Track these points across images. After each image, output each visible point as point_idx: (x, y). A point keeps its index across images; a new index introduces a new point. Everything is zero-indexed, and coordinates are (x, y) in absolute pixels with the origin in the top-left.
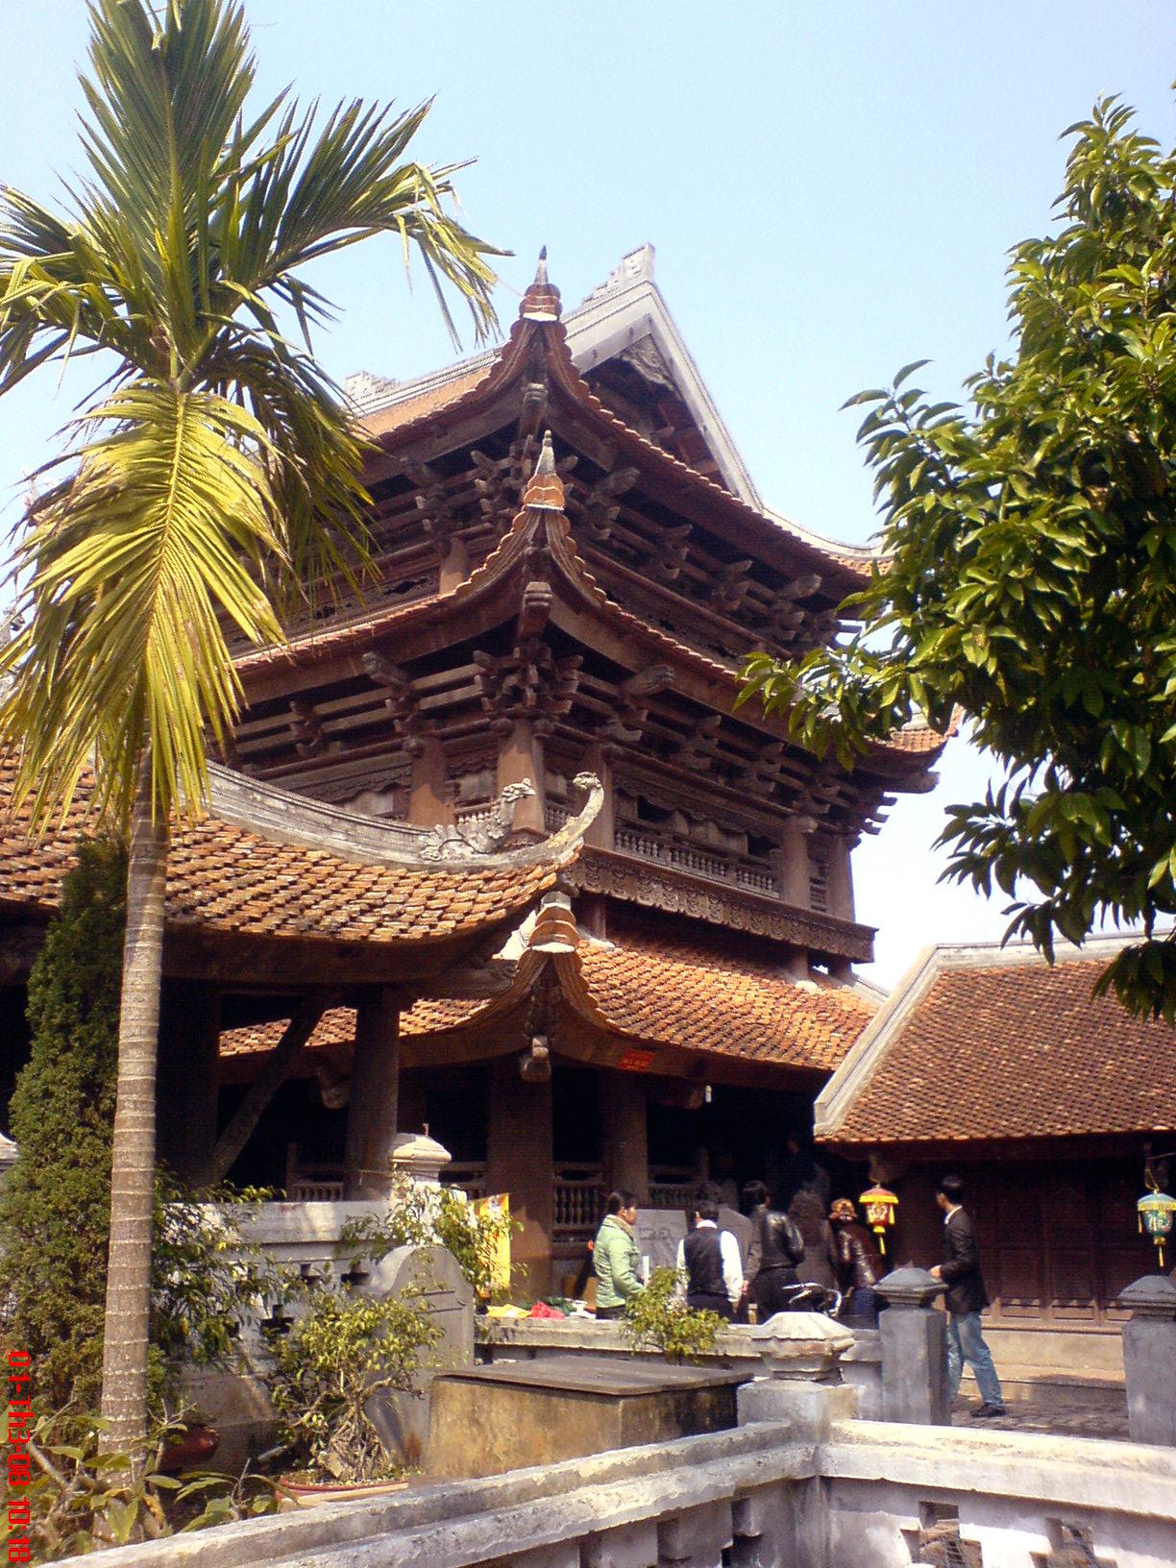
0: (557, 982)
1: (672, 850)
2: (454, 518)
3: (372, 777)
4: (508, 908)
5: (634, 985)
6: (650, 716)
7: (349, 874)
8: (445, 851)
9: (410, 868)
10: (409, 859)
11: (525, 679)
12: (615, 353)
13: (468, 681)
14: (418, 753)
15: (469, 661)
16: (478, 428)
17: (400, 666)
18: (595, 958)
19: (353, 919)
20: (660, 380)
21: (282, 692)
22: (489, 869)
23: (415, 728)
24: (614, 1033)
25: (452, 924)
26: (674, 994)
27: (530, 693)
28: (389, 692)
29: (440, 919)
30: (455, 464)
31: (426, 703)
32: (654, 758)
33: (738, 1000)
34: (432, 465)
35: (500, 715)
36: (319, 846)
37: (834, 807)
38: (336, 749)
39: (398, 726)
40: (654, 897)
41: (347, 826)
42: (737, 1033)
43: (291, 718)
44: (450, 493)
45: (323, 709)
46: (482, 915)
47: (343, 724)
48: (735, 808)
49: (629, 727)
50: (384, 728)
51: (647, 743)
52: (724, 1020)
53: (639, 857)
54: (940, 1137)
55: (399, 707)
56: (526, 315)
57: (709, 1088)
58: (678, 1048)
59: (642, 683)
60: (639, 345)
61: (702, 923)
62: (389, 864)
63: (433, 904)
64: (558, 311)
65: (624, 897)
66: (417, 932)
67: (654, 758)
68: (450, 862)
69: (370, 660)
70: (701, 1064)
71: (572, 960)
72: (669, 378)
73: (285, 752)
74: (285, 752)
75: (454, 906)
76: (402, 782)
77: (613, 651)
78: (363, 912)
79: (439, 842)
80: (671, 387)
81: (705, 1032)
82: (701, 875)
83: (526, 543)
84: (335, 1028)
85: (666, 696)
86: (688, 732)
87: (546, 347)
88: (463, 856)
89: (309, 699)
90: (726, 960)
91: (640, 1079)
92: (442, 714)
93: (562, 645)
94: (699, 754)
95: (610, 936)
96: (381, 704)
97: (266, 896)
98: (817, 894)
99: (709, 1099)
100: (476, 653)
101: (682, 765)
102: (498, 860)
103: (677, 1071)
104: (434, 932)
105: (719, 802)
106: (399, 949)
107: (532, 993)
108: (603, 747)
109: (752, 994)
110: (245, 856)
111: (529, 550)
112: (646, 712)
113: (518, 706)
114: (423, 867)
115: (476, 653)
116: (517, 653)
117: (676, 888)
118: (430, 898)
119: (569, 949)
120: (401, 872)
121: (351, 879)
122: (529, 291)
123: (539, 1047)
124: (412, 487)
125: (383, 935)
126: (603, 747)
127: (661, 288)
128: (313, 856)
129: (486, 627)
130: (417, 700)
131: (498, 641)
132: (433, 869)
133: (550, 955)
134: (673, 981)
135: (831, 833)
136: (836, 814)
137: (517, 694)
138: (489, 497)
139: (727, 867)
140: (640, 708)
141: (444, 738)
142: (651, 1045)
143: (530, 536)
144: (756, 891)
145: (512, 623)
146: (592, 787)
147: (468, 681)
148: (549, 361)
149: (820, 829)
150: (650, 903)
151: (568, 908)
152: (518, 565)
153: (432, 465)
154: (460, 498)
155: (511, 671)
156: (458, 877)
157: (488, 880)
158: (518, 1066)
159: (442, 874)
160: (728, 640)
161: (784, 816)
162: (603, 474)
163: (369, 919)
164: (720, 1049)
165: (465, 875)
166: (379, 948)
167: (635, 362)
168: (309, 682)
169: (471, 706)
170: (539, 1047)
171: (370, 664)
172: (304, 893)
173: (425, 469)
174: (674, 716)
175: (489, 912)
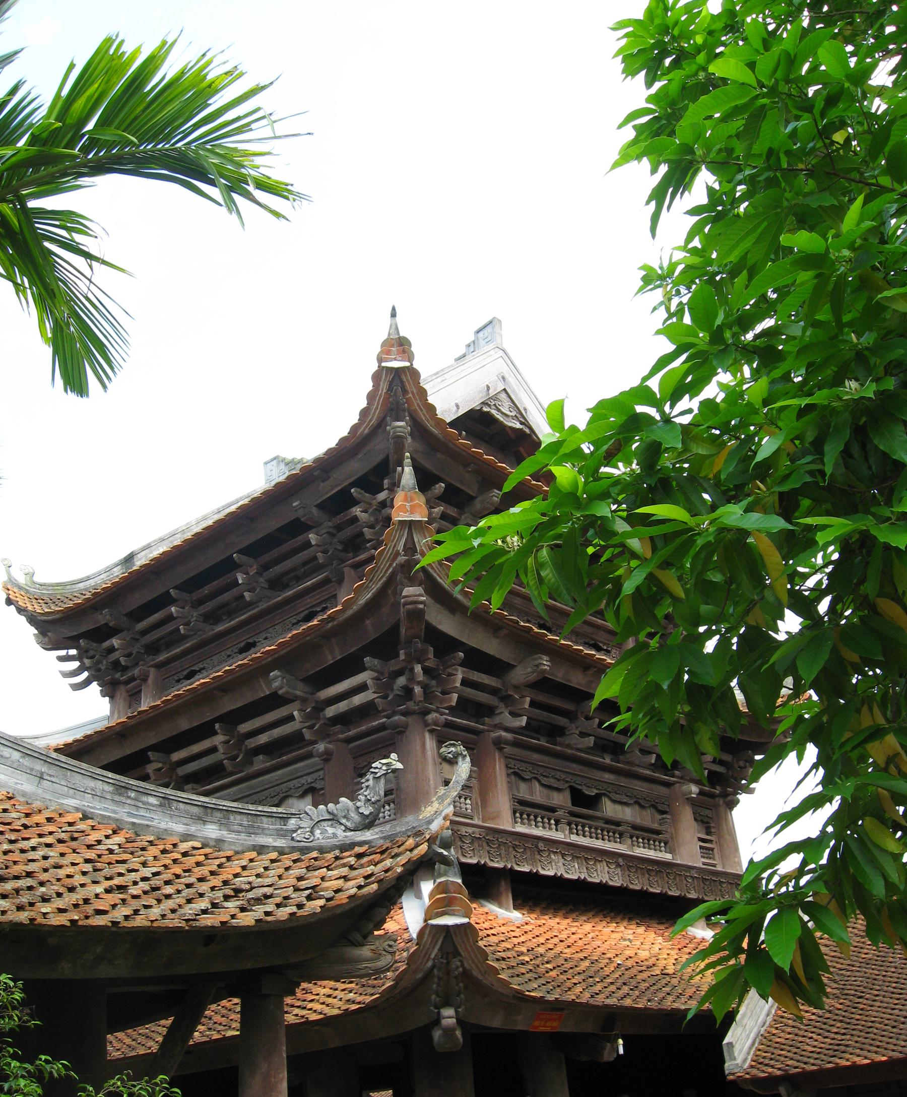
0: (457, 954)
1: (569, 824)
2: (345, 550)
3: (291, 784)
4: (380, 882)
5: (541, 950)
6: (533, 704)
7: (217, 862)
8: (317, 832)
9: (281, 852)
10: (281, 843)
11: (412, 679)
12: (474, 404)
13: (362, 688)
14: (327, 757)
15: (362, 669)
16: (356, 468)
17: (305, 680)
18: (503, 929)
19: (214, 905)
20: (518, 426)
21: (209, 716)
22: (361, 844)
23: (323, 735)
24: (521, 998)
25: (322, 902)
26: (581, 955)
27: (417, 689)
28: (297, 704)
29: (309, 898)
30: (342, 501)
31: (331, 711)
32: (543, 742)
33: (644, 954)
34: (320, 506)
35: (394, 713)
36: (186, 837)
37: (711, 773)
38: (260, 762)
39: (308, 735)
40: (554, 867)
41: (218, 815)
42: (643, 986)
43: (218, 740)
44: (339, 528)
45: (245, 728)
46: (353, 891)
47: (263, 739)
48: (623, 782)
49: (514, 714)
50: (296, 739)
51: (532, 728)
52: (635, 973)
53: (538, 832)
54: (844, 1063)
55: (307, 717)
56: (383, 364)
57: (621, 1041)
58: (586, 1005)
59: (522, 674)
60: (495, 397)
61: (602, 888)
62: (261, 849)
63: (303, 884)
64: (410, 358)
65: (526, 869)
66: (283, 913)
67: (543, 742)
68: (323, 842)
69: (276, 677)
70: (611, 1018)
71: (467, 930)
72: (525, 423)
73: (216, 771)
74: (216, 771)
75: (326, 884)
76: (317, 786)
77: (491, 647)
78: (227, 898)
79: (311, 823)
80: (527, 431)
81: (613, 988)
82: (598, 844)
83: (397, 554)
84: (222, 1020)
85: (543, 684)
86: (571, 716)
87: (405, 391)
88: (335, 835)
89: (232, 719)
90: (630, 919)
91: (557, 1039)
92: (344, 719)
93: (444, 645)
94: (583, 735)
95: (518, 905)
96: (291, 718)
97: (122, 888)
98: (707, 852)
99: (621, 1051)
100: (367, 659)
101: (568, 746)
102: (367, 835)
103: (588, 1027)
104: (301, 913)
105: (607, 777)
106: (263, 933)
107: (433, 967)
108: (494, 735)
109: (656, 948)
110: (111, 851)
111: (402, 559)
112: (528, 699)
113: (410, 704)
114: (293, 849)
115: (367, 659)
116: (402, 656)
117: (575, 857)
118: (300, 879)
119: (466, 920)
120: (274, 855)
121: (220, 866)
122: (384, 344)
123: (449, 1016)
124: (308, 528)
125: (247, 920)
126: (494, 735)
127: (508, 351)
128: (184, 846)
129: (373, 635)
130: (323, 710)
131: (385, 646)
132: (304, 850)
133: (446, 928)
134: (580, 943)
135: (712, 796)
136: (714, 778)
137: (408, 692)
138: (372, 527)
139: (621, 835)
140: (523, 697)
141: (349, 741)
142: (558, 1006)
143: (400, 547)
144: (651, 854)
145: (395, 628)
146: (457, 755)
147: (362, 688)
148: (408, 401)
149: (701, 793)
150: (551, 873)
151: (460, 881)
152: (393, 575)
153: (320, 506)
154: (348, 532)
155: (400, 673)
156: (330, 856)
157: (359, 856)
158: (431, 1038)
159: (314, 854)
160: (601, 637)
161: (668, 785)
162: (471, 498)
163: (232, 905)
164: (628, 1002)
165: (337, 852)
166: (244, 933)
167: (494, 412)
168: (229, 704)
169: (367, 710)
170: (449, 1016)
171: (277, 681)
172: (167, 883)
173: (315, 511)
174: (557, 703)
175: (360, 887)
